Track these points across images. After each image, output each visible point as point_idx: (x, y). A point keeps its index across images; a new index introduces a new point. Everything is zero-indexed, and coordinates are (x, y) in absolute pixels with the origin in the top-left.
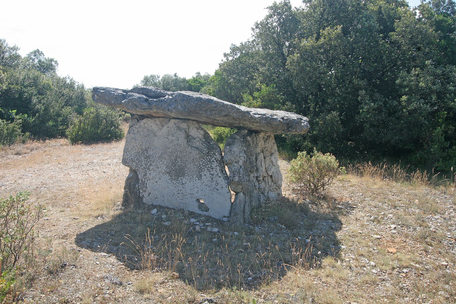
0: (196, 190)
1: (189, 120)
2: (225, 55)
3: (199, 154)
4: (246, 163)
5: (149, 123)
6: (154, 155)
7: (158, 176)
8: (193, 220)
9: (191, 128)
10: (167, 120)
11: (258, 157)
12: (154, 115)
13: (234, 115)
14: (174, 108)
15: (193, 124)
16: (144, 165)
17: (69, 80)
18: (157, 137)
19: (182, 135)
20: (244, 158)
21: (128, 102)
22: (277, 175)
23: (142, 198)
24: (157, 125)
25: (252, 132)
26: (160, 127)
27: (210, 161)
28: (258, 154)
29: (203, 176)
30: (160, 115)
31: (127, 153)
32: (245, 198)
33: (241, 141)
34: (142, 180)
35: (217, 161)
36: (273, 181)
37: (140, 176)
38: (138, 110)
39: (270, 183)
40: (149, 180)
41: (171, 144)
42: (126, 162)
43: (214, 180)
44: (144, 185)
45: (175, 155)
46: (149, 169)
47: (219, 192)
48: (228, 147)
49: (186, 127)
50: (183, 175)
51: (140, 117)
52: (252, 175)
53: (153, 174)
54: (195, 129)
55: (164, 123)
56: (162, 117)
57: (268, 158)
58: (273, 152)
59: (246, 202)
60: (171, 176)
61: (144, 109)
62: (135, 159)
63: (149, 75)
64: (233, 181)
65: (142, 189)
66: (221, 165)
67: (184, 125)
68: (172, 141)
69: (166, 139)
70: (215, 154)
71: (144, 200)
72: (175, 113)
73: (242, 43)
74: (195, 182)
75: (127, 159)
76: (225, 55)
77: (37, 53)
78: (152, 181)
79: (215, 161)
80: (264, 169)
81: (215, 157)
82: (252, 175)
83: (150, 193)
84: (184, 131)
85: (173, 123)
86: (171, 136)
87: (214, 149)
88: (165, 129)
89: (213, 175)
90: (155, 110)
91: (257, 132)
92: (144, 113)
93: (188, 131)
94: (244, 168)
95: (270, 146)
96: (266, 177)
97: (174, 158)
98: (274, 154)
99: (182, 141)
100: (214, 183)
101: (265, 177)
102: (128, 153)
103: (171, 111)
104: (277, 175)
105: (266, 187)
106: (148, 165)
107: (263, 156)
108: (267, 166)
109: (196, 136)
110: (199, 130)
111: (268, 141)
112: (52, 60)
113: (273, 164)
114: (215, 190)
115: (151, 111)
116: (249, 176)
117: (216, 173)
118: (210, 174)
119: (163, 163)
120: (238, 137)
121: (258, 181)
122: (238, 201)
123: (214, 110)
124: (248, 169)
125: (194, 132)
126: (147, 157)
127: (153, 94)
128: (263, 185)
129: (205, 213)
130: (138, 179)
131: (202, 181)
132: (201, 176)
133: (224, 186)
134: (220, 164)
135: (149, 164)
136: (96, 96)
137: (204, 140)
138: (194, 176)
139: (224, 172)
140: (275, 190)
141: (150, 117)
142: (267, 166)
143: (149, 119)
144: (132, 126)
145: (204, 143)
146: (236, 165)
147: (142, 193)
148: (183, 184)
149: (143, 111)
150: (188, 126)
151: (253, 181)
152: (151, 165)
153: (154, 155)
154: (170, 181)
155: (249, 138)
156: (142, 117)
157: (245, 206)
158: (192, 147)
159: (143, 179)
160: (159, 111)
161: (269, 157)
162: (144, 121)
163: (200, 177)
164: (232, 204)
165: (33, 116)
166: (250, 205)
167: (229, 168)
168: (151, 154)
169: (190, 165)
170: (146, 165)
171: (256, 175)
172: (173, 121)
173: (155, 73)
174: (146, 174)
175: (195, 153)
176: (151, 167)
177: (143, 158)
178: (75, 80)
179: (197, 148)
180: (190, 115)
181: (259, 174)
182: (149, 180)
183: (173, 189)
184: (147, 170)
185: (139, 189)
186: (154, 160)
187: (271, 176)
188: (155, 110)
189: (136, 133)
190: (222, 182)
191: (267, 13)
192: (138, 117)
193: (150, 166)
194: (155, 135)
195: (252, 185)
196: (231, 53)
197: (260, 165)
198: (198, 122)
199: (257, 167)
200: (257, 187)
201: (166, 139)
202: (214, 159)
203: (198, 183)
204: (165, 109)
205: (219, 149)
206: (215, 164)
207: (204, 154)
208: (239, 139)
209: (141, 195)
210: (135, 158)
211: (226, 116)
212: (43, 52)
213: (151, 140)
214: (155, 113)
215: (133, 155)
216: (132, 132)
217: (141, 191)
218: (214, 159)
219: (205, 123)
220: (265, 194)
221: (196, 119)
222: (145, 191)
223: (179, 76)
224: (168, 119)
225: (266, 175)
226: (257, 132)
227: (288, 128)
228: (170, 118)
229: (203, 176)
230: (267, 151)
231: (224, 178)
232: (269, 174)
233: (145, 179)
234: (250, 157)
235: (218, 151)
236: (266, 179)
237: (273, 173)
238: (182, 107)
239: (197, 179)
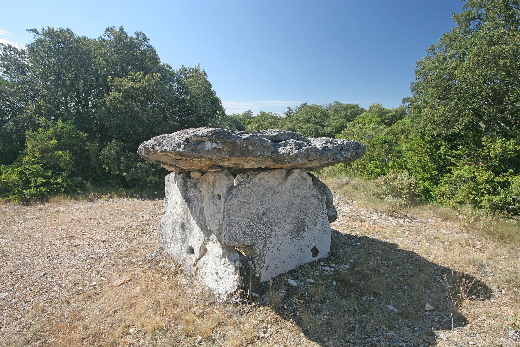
5: (266, 177)
6: (274, 217)
18: (279, 194)
24: (277, 178)
31: (236, 227)
62: (250, 230)
69: (291, 194)
75: (237, 234)
86: (296, 189)
106: (268, 232)
153: (274, 217)
162: (259, 176)
168: (270, 216)
183: (293, 248)
184: (266, 239)
193: (271, 232)
210: (249, 229)
215: (243, 227)
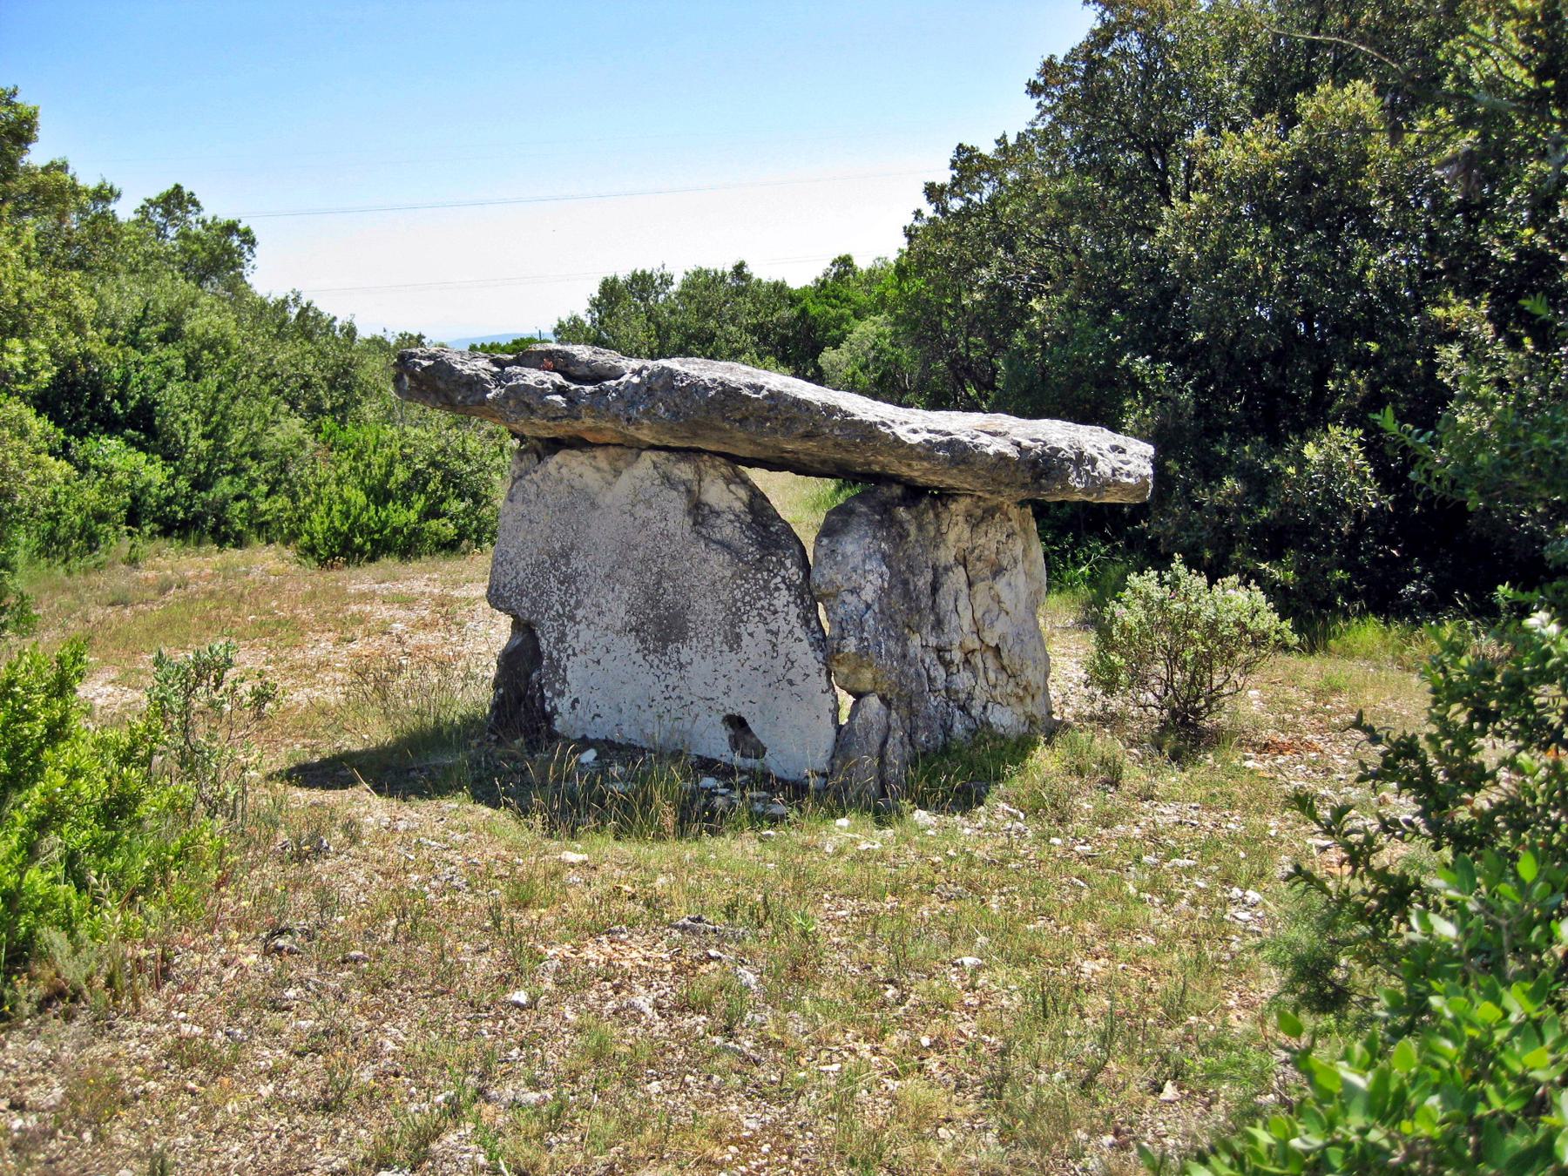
0: (722, 683)
1: (699, 451)
2: (933, 192)
3: (731, 564)
4: (888, 595)
5: (574, 464)
7: (602, 641)
8: (709, 782)
9: (707, 480)
10: (630, 454)
11: (942, 580)
12: (589, 437)
13: (837, 432)
14: (646, 413)
15: (714, 467)
16: (557, 606)
17: (296, 311)
19: (676, 503)
20: (881, 576)
21: (506, 397)
22: (1017, 649)
23: (549, 718)
24: (598, 470)
25: (915, 493)
26: (610, 478)
27: (765, 588)
28: (947, 569)
29: (745, 637)
30: (607, 439)
32: (888, 716)
33: (870, 523)
34: (550, 657)
35: (788, 589)
36: (1003, 668)
37: (543, 643)
38: (536, 421)
39: (992, 675)
40: (575, 654)
41: (644, 533)
42: (501, 596)
43: (782, 649)
44: (556, 673)
45: (655, 570)
46: (572, 618)
47: (794, 689)
48: (825, 541)
49: (691, 476)
50: (682, 636)
51: (546, 448)
52: (916, 641)
53: (586, 635)
54: (721, 484)
55: (621, 464)
56: (614, 445)
57: (980, 587)
58: (1005, 563)
59: (889, 727)
60: (643, 641)
61: (554, 419)
63: (623, 275)
64: (838, 651)
65: (552, 687)
66: (803, 601)
67: (684, 471)
68: (645, 524)
69: (627, 516)
70: (782, 564)
71: (558, 724)
72: (650, 429)
73: (1002, 141)
74: (719, 659)
76: (933, 192)
77: (176, 201)
78: (581, 657)
79: (782, 586)
80: (966, 623)
81: (783, 572)
82: (916, 641)
83: (576, 700)
84: (682, 488)
85: (648, 463)
87: (781, 547)
88: (625, 483)
89: (776, 634)
90: (589, 422)
91: (944, 496)
92: (560, 432)
93: (696, 488)
94: (882, 612)
95: (994, 546)
96: (978, 655)
97: (650, 579)
98: (1007, 574)
99: (678, 522)
100: (782, 659)
101: (973, 651)
102: (507, 566)
103: (637, 424)
104: (1017, 649)
105: (978, 688)
107: (963, 578)
108: (978, 615)
109: (723, 506)
110: (732, 487)
111: (983, 527)
112: (231, 228)
113: (1001, 609)
114: (784, 684)
115: (577, 425)
116: (903, 640)
117: (785, 628)
118: (768, 631)
119: (619, 598)
120: (864, 509)
121: (947, 665)
122: (858, 721)
123: (768, 419)
124: (898, 617)
125: (717, 493)
126: (567, 580)
127: (579, 371)
128: (963, 680)
129: (750, 762)
130: (537, 655)
131: (742, 656)
132: (738, 636)
133: (812, 671)
134: (801, 596)
135: (572, 602)
136: (406, 378)
137: (749, 519)
138: (718, 639)
139: (813, 624)
140: (1013, 700)
141: (577, 443)
142: (978, 615)
143: (574, 452)
144: (520, 477)
145: (749, 527)
146: (849, 598)
147: (551, 699)
148: (681, 666)
149: (551, 424)
150: (698, 471)
151: (923, 661)
152: (578, 604)
154: (639, 658)
155: (902, 513)
156: (555, 445)
157: (884, 743)
158: (709, 540)
159: (555, 653)
160: (602, 424)
161: (989, 582)
162: (558, 458)
163: (734, 641)
164: (839, 728)
165: (493, 375)
166: (906, 739)
167: (826, 609)
169: (702, 602)
170: (563, 605)
171: (932, 641)
172: (648, 457)
173: (647, 263)
174: (564, 635)
175: (718, 564)
176: (580, 613)
177: (554, 583)
178: (321, 309)
179: (725, 546)
180: (695, 435)
181: (944, 639)
182: (575, 654)
185: (541, 688)
186: (590, 589)
187: (997, 650)
188: (589, 422)
189: (532, 498)
190: (805, 655)
191: (578, 303)
192: (539, 446)
194: (594, 505)
195: (919, 675)
196: (956, 182)
197: (951, 606)
198: (734, 460)
199: (937, 615)
200: (940, 684)
201: (627, 516)
202: (779, 579)
203: (730, 661)
204: (617, 416)
205: (796, 548)
206: (783, 598)
207: (747, 563)
208: (866, 514)
209: (548, 709)
211: (808, 436)
212: (198, 197)
213: (579, 522)
214: (590, 429)
215: (522, 574)
216: (519, 497)
217: (548, 694)
218: (779, 579)
219: (752, 463)
220: (973, 712)
221: (722, 449)
222: (561, 694)
223: (756, 276)
224: (635, 451)
225: (977, 645)
226: (944, 496)
227: (1036, 478)
228: (639, 447)
229: (746, 639)
230: (979, 559)
231: (811, 645)
232: (987, 640)
233: (559, 652)
234: (907, 575)
235: (792, 555)
236: (977, 660)
237: (1003, 637)
238: (667, 410)
239: (725, 648)
